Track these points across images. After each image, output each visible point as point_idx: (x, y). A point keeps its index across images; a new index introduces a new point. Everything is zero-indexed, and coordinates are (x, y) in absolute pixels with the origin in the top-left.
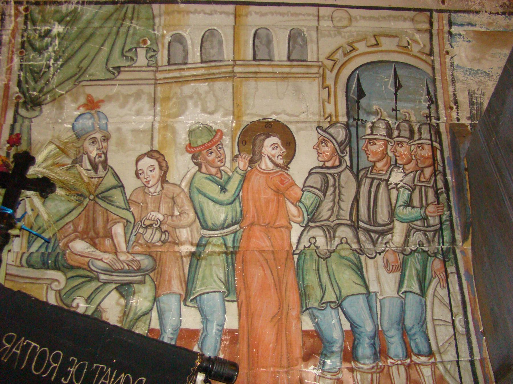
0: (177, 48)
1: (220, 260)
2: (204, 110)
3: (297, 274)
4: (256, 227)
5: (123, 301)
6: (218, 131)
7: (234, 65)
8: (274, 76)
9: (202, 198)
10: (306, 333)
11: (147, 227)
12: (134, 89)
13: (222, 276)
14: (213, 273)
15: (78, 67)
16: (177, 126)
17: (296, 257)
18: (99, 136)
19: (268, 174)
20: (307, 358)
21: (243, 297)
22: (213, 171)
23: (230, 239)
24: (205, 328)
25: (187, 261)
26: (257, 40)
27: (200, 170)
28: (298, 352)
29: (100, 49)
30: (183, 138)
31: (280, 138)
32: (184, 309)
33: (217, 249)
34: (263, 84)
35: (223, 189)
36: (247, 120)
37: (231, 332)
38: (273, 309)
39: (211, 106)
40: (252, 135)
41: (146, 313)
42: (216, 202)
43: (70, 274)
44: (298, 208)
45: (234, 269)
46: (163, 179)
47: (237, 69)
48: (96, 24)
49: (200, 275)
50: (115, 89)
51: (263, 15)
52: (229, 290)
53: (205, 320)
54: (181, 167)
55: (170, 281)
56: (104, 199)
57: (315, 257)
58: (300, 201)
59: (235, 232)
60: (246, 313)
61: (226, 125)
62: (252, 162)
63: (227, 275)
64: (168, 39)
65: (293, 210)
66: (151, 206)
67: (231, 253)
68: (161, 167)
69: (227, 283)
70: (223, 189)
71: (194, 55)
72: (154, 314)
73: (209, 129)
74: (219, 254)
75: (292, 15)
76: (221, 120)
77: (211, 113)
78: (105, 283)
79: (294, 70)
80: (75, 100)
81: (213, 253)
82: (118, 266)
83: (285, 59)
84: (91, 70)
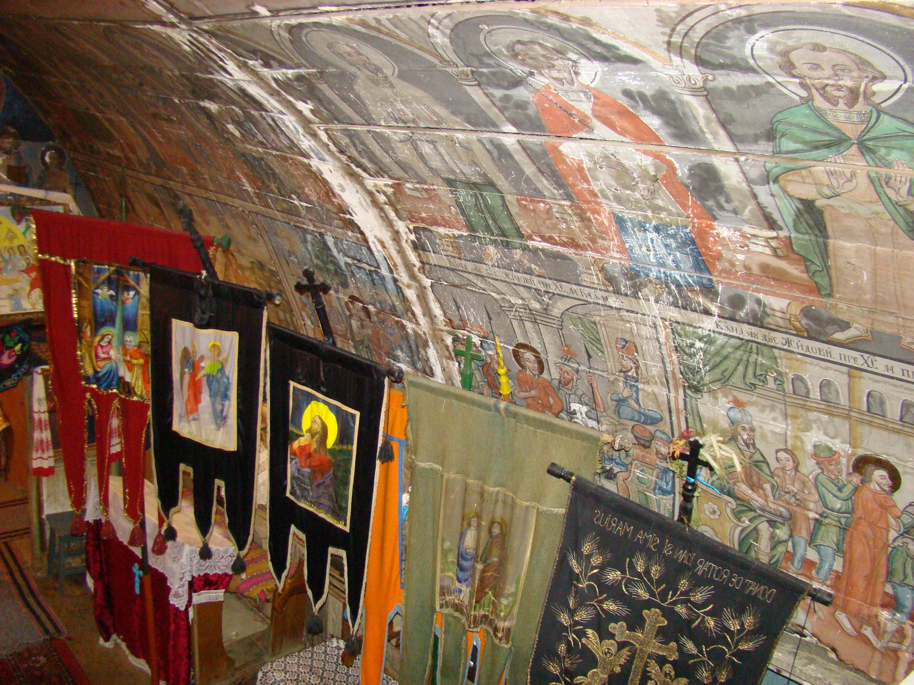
0: (798, 384)
1: (835, 530)
2: (826, 434)
3: (888, 560)
4: (863, 521)
5: (771, 530)
6: (836, 452)
7: (850, 411)
8: (886, 428)
9: (824, 489)
10: (886, 593)
11: (786, 492)
12: (770, 403)
13: (835, 539)
14: (830, 536)
15: (722, 374)
16: (805, 438)
17: (890, 549)
18: (747, 426)
19: (874, 493)
20: (884, 606)
21: (848, 555)
22: (833, 477)
23: (843, 521)
24: (821, 563)
25: (812, 523)
26: (870, 399)
27: (823, 473)
28: (878, 600)
29: (735, 369)
30: (809, 448)
31: (888, 473)
32: (809, 549)
33: (834, 523)
34: (875, 431)
35: (840, 490)
36: (861, 452)
37: (837, 572)
38: (867, 571)
39: (832, 433)
40: (862, 464)
41: (786, 541)
42: (835, 496)
43: (738, 502)
44: (897, 522)
45: (844, 539)
46: (796, 469)
47: (852, 413)
48: (729, 350)
49: (820, 534)
50: (754, 399)
51: (826, 369)
52: (839, 550)
53: (821, 560)
54: (809, 467)
55: (800, 529)
56: (757, 466)
57: (905, 554)
58: (899, 518)
59: (847, 518)
60: (848, 564)
61: (844, 451)
62: (863, 482)
63: (838, 540)
64: (791, 376)
65: (892, 521)
66: (788, 482)
67: (844, 529)
68: (794, 461)
69: (837, 545)
70: (840, 490)
71: (815, 394)
72: (790, 544)
73: (830, 449)
74: (835, 526)
75: (906, 389)
76: (840, 446)
77: (832, 438)
78: (760, 515)
79: (906, 429)
80: (726, 396)
81: (830, 524)
82: (768, 509)
83: (898, 419)
84: (733, 380)
